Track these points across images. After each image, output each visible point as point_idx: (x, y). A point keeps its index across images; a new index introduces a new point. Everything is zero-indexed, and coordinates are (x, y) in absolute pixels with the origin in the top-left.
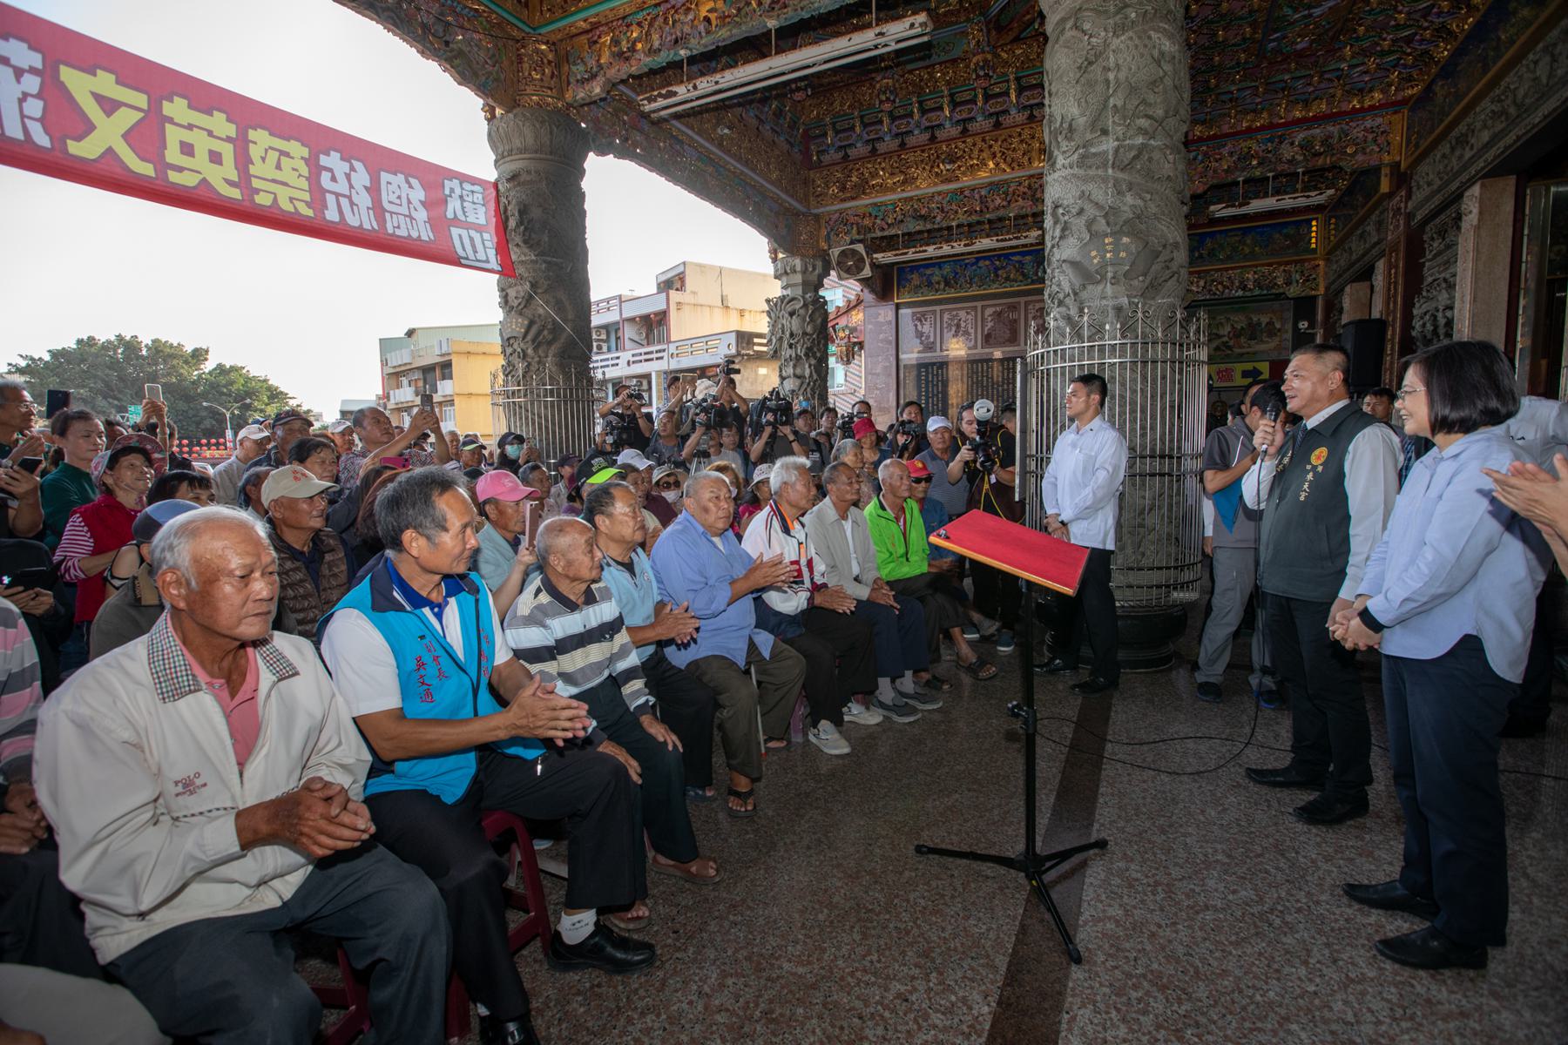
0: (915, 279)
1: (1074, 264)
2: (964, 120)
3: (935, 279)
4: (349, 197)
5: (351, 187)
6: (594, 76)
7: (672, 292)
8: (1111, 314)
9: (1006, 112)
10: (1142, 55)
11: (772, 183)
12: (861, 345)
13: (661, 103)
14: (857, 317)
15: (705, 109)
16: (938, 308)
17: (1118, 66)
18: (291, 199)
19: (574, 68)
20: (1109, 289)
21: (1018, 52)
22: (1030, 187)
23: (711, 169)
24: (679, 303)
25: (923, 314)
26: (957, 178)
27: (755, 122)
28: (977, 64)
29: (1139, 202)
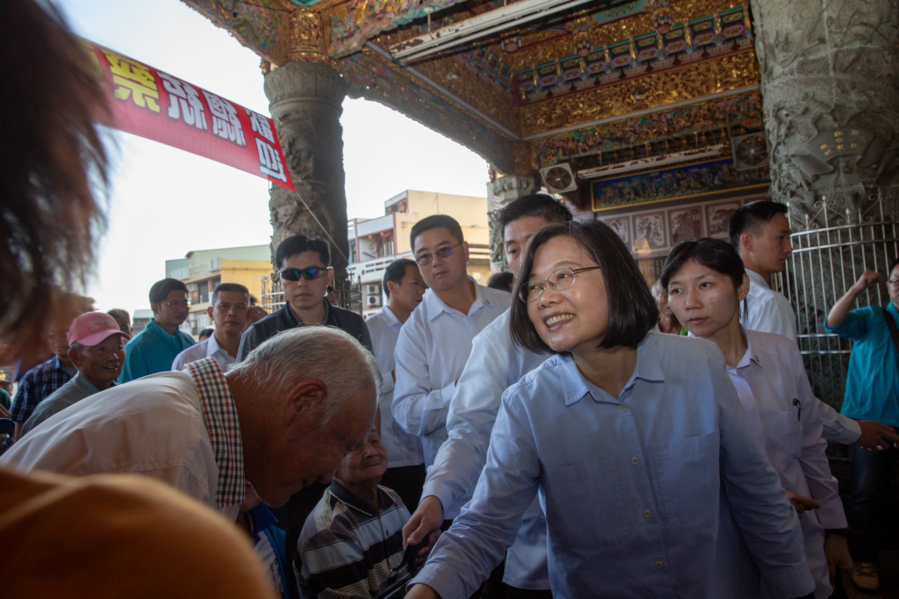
0: (609, 192)
1: (806, 158)
2: (648, 61)
3: (626, 190)
4: (187, 100)
5: (186, 94)
6: (351, 35)
7: (398, 214)
8: (849, 199)
9: (683, 52)
11: (492, 117)
13: (409, 50)
15: (435, 57)
16: (630, 214)
18: (144, 95)
19: (335, 30)
20: (843, 178)
22: (709, 110)
23: (442, 107)
24: (403, 223)
25: (618, 220)
26: (646, 106)
27: (475, 70)
28: (658, 16)
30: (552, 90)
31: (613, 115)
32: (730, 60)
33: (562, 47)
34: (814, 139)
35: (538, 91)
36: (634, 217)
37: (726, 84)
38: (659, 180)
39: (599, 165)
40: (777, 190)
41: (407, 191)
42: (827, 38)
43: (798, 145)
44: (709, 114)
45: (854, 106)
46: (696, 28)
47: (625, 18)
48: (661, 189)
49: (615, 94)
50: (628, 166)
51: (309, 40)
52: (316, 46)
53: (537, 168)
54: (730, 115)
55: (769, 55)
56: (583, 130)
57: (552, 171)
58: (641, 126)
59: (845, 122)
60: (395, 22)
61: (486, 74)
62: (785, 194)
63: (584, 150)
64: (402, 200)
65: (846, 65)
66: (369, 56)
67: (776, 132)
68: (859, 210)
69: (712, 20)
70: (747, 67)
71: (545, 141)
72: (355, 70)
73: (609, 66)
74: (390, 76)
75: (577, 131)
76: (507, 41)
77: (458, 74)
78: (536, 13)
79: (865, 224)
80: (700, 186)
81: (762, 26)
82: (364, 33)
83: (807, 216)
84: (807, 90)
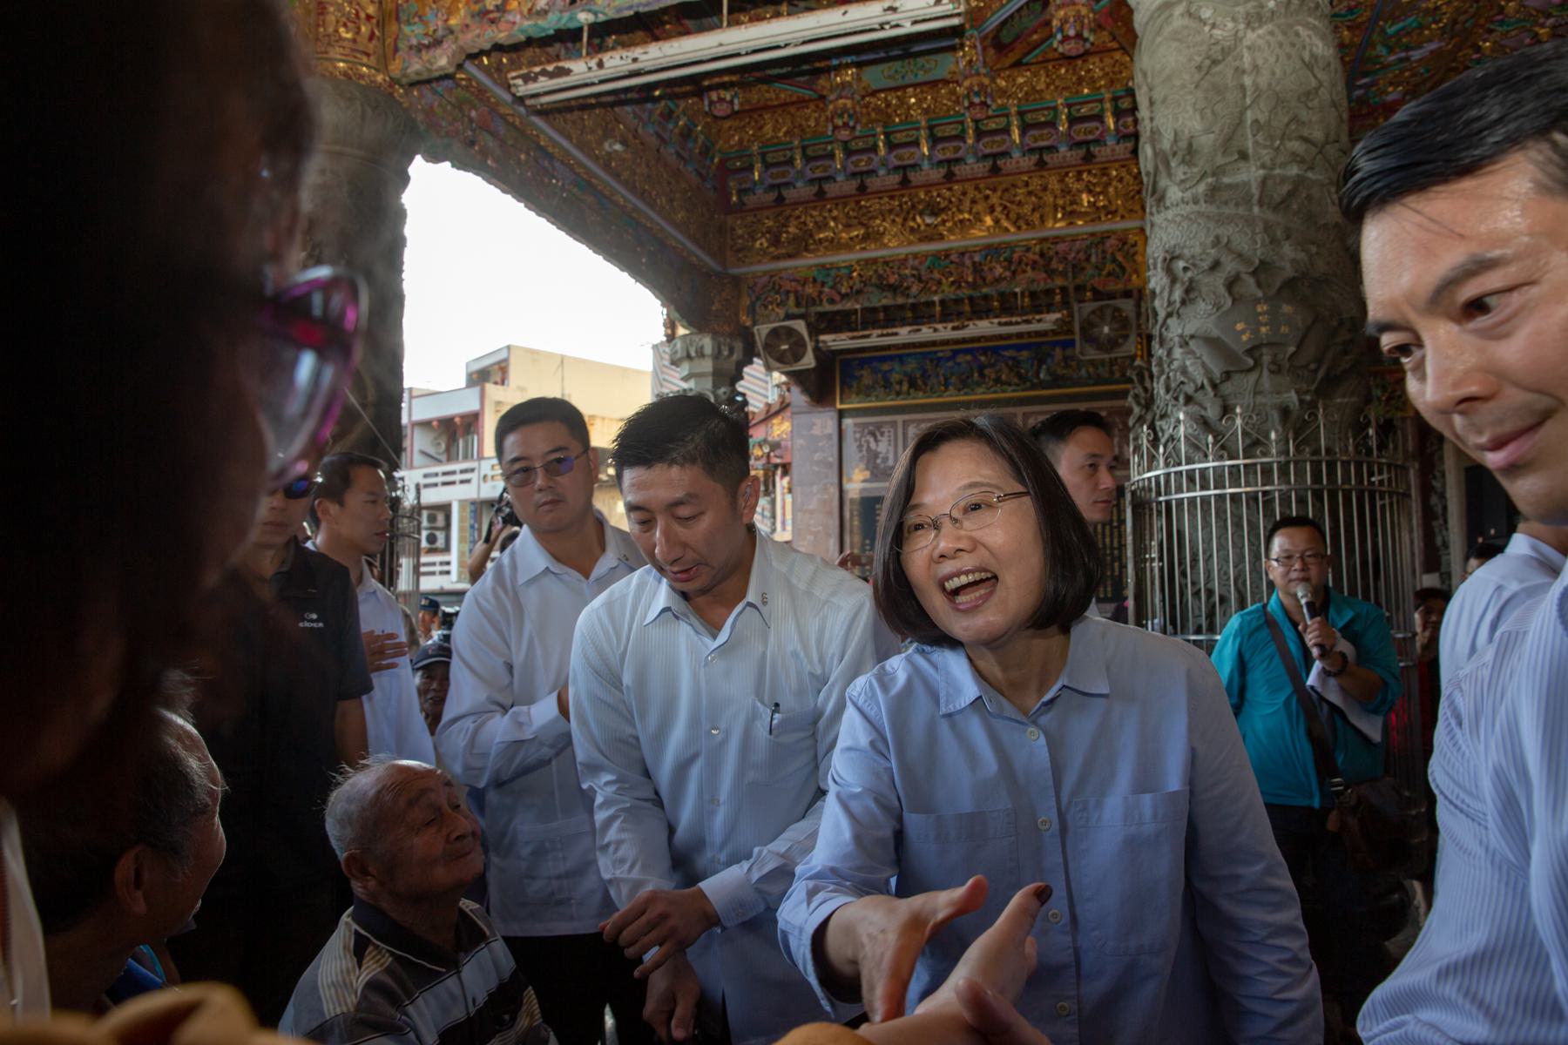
0: (867, 376)
1: (1213, 343)
2: (949, 161)
3: (895, 377)
6: (437, 43)
7: (489, 387)
8: (1276, 416)
9: (1006, 154)
10: (1289, 57)
12: (786, 469)
13: (544, 84)
14: (780, 428)
15: (583, 105)
16: (899, 418)
17: (1256, 67)
19: (407, 30)
20: (1266, 381)
21: (1021, 80)
22: (1042, 255)
23: (590, 199)
25: (879, 426)
26: (941, 237)
27: (654, 141)
28: (970, 89)
29: (1301, 256)
30: (785, 192)
31: (885, 246)
32: (1079, 179)
33: (807, 120)
34: (1227, 313)
35: (759, 191)
36: (906, 424)
37: (1071, 215)
38: (950, 364)
39: (856, 330)
40: (1162, 392)
41: (508, 347)
42: (1250, 151)
43: (1199, 319)
44: (1041, 262)
45: (1288, 265)
46: (1028, 118)
47: (915, 86)
48: (953, 380)
49: (891, 211)
50: (904, 334)
51: (354, 41)
52: (368, 55)
53: (748, 323)
54: (1074, 266)
55: (1161, 167)
56: (834, 266)
57: (774, 333)
58: (930, 270)
59: (1273, 291)
60: (522, 31)
61: (672, 150)
62: (1176, 399)
63: (832, 301)
64: (499, 363)
65: (1277, 199)
66: (466, 88)
67: (1166, 294)
68: (1291, 435)
69: (1055, 109)
70: (1104, 192)
71: (766, 278)
72: (438, 111)
73: (884, 163)
74: (502, 130)
75: (823, 266)
76: (714, 96)
77: (624, 142)
78: (778, 47)
79: (1299, 457)
80: (1016, 380)
81: (1152, 119)
82: (461, 42)
83: (1210, 439)
84: (1219, 231)
